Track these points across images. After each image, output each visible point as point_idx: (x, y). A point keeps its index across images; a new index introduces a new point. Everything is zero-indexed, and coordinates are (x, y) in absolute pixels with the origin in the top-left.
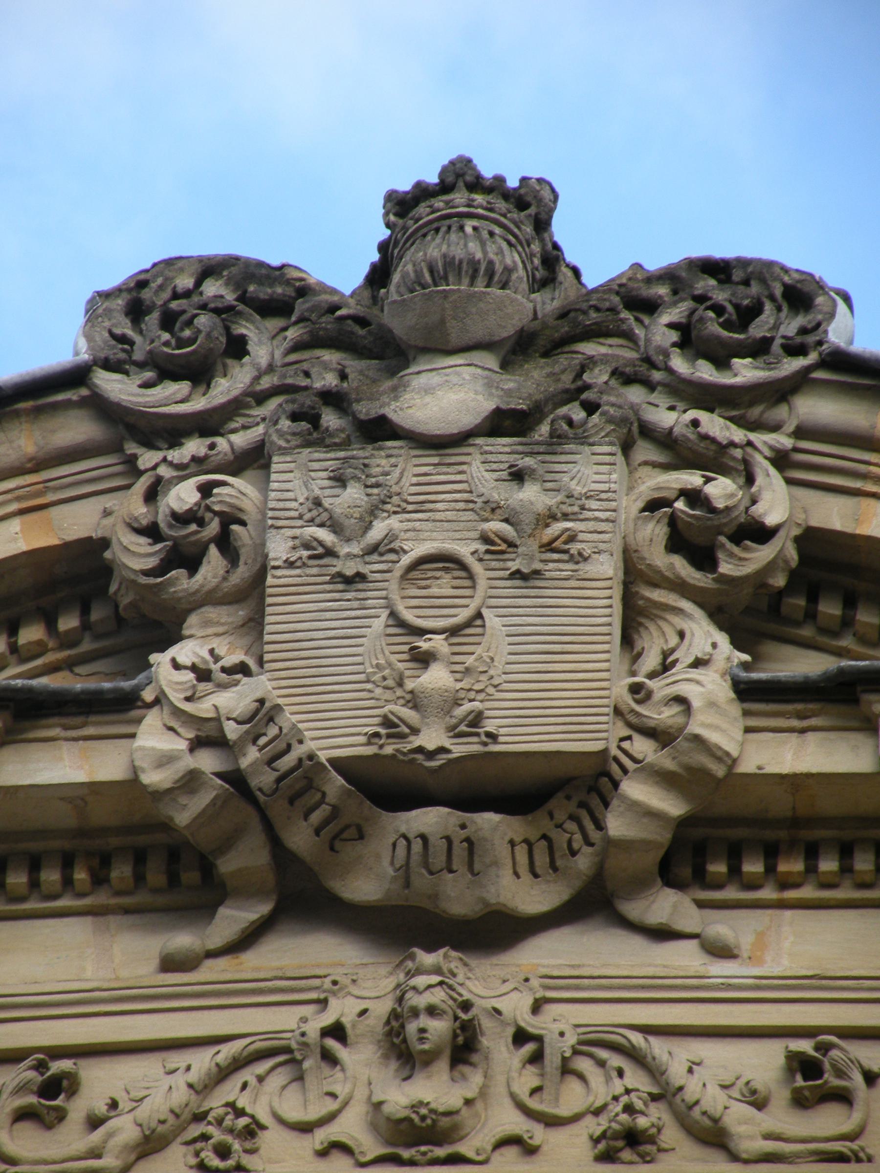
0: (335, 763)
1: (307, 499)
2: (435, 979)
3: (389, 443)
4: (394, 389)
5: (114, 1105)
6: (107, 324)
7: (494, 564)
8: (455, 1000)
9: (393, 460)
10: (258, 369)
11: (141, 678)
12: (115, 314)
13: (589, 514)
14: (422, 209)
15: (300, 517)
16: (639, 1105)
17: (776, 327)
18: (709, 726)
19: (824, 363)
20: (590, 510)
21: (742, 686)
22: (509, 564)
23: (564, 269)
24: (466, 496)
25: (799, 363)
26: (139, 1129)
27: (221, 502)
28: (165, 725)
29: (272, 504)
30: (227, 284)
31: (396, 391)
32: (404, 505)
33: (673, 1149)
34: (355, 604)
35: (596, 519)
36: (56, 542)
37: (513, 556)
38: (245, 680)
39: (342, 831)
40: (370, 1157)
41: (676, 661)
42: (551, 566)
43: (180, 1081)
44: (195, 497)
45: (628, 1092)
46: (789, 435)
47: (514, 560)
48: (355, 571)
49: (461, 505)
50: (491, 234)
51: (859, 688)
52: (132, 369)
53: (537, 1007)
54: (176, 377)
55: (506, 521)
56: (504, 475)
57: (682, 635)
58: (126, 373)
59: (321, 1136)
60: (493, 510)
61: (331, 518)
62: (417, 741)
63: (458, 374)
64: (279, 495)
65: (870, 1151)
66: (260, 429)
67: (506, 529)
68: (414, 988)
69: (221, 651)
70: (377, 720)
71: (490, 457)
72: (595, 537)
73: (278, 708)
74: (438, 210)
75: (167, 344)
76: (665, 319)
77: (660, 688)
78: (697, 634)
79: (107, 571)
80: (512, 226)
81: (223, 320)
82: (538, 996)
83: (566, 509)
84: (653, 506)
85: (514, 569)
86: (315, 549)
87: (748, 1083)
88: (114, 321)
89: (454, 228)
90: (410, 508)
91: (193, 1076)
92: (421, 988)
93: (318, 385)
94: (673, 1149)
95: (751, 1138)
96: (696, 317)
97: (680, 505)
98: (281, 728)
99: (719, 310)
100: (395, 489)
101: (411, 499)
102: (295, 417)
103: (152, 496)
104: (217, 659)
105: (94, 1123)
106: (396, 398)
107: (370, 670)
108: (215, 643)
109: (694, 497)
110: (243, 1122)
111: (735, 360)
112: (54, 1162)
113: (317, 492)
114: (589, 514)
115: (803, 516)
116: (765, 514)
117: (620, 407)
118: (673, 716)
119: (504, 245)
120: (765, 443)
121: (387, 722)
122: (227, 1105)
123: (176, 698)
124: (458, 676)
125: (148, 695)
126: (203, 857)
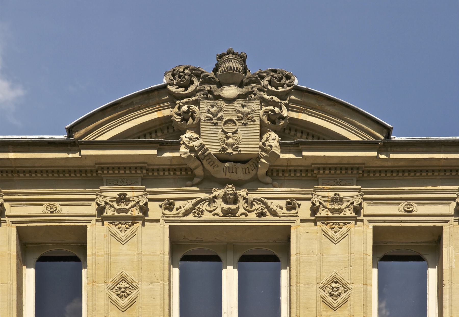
0: (214, 154)
1: (207, 109)
2: (231, 189)
3: (220, 100)
4: (221, 90)
5: (180, 207)
6: (169, 77)
7: (239, 121)
8: (234, 192)
9: (221, 103)
10: (196, 86)
11: (180, 139)
12: (170, 75)
13: (255, 113)
14: (224, 57)
15: (206, 112)
16: (263, 208)
17: (285, 82)
18: (275, 150)
19: (293, 89)
20: (255, 112)
21: (280, 143)
22: (242, 121)
23: (247, 70)
24: (234, 109)
25: (290, 88)
26: (185, 211)
27: (191, 110)
28: (253, 158)
29: (201, 110)
30: (189, 71)
31: (221, 91)
32: (224, 111)
33: (268, 215)
34: (216, 128)
35: (257, 114)
36: (163, 116)
37: (242, 120)
38: (198, 140)
39: (215, 166)
40: (221, 216)
41: (269, 139)
42: (249, 122)
43: (191, 204)
44: (187, 108)
45: (261, 207)
46: (288, 101)
47: (243, 121)
48: (216, 122)
49: (234, 111)
50: (237, 62)
51: (299, 144)
52: (174, 86)
53: (247, 194)
54: (182, 87)
55: (241, 114)
56: (241, 106)
57: (270, 135)
58: (173, 86)
59: (213, 213)
60: (239, 112)
61: (211, 113)
62: (227, 151)
63: (232, 88)
64: (202, 108)
65: (298, 215)
66: (197, 97)
67: (242, 115)
68: (228, 191)
69: (193, 135)
70: (221, 147)
71: (238, 103)
72: (256, 117)
73: (204, 145)
74: (227, 57)
75: (180, 81)
76: (266, 79)
77: (267, 143)
78: (273, 135)
79: (172, 121)
80: (240, 61)
81: (189, 77)
82: (247, 192)
83: (251, 112)
84: (265, 112)
85: (243, 122)
86: (209, 118)
87: (280, 206)
88: (170, 77)
89: (230, 61)
90: (225, 111)
91: (192, 203)
92: (229, 191)
93: (206, 89)
94: (268, 215)
95: (281, 213)
96: (272, 79)
97: (270, 112)
98: (205, 148)
99: (276, 78)
100: (222, 108)
101: (225, 110)
102: (203, 95)
103: (179, 108)
104: (192, 137)
105: (177, 209)
106: (222, 92)
107: (219, 139)
108: (191, 134)
109: (273, 111)
110: (201, 210)
111: (279, 87)
112: (172, 215)
113: (209, 108)
114: (255, 113)
115: (290, 115)
116: (284, 115)
117: (260, 95)
118: (269, 148)
119: (239, 64)
120: (284, 102)
121: (223, 148)
122: (198, 207)
123: (186, 143)
124: (234, 140)
125: (181, 142)
126: (191, 169)
